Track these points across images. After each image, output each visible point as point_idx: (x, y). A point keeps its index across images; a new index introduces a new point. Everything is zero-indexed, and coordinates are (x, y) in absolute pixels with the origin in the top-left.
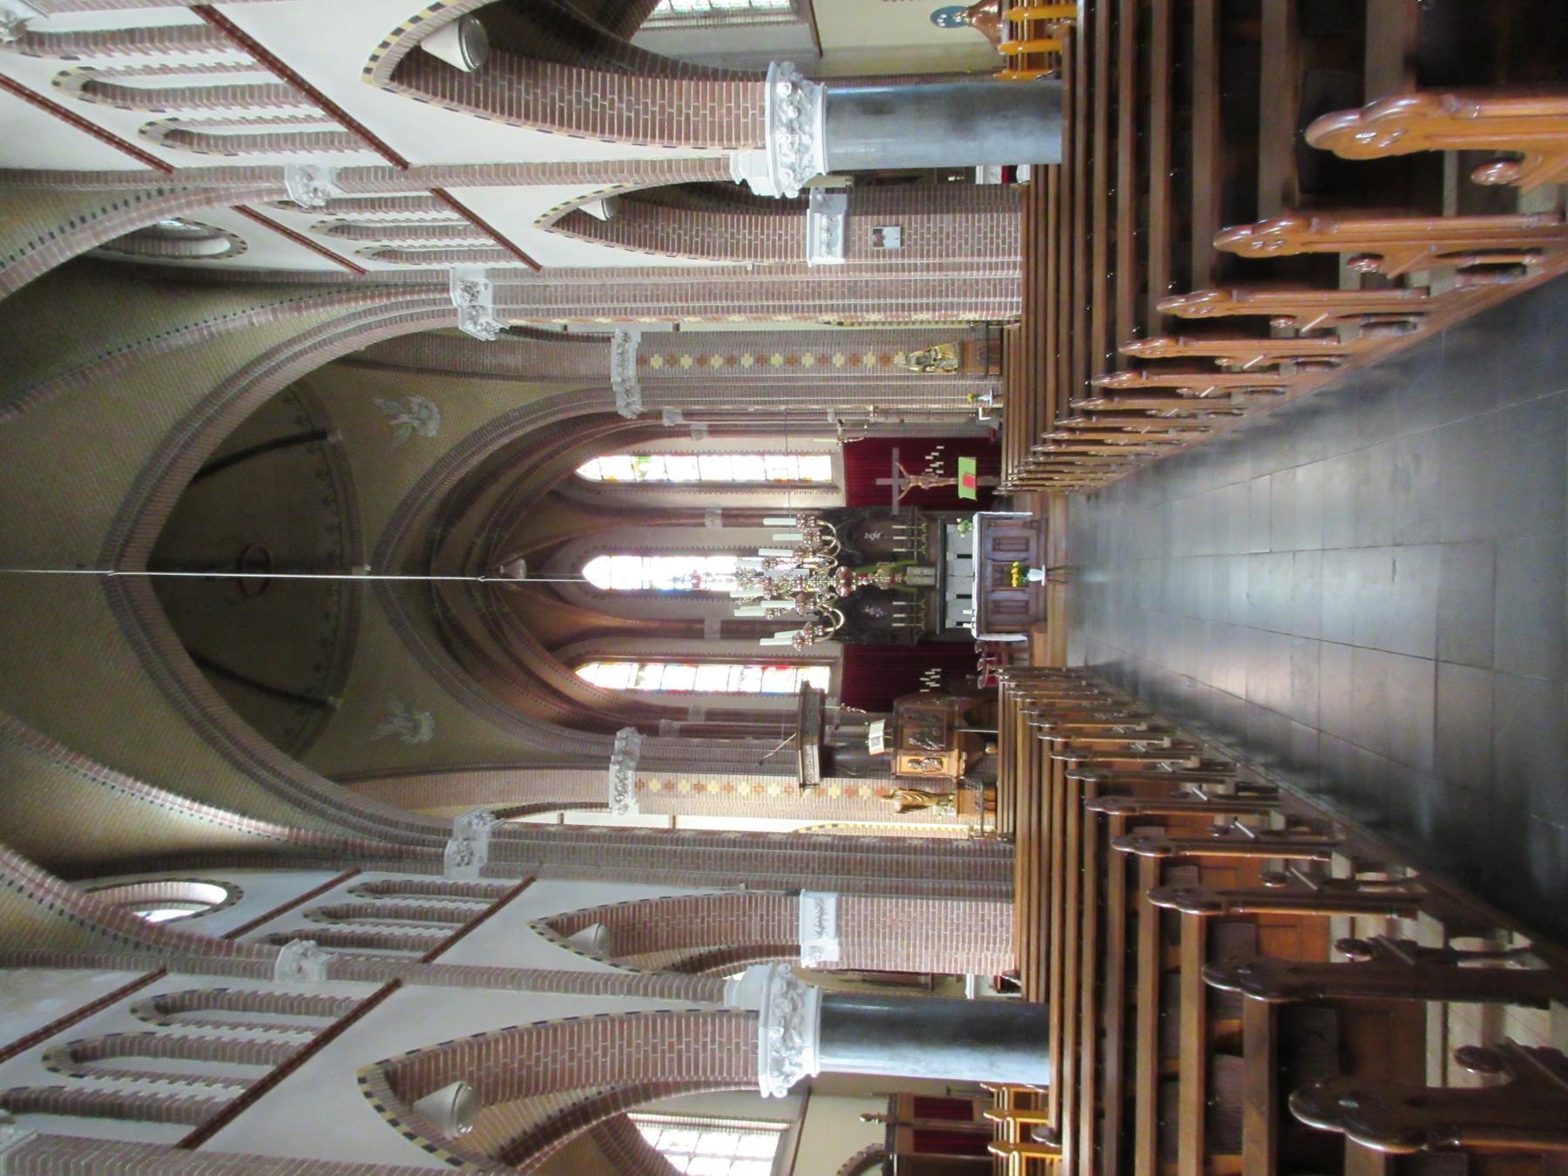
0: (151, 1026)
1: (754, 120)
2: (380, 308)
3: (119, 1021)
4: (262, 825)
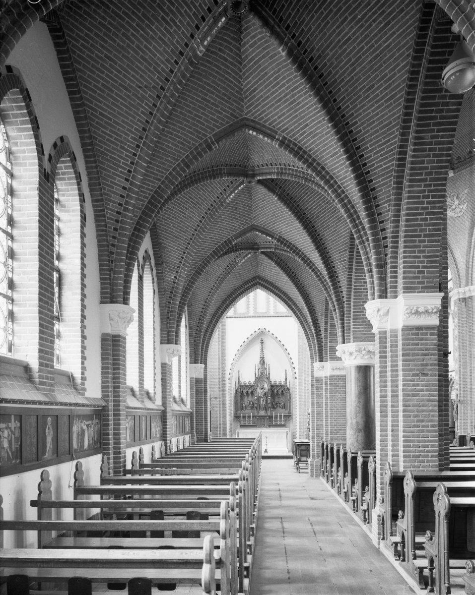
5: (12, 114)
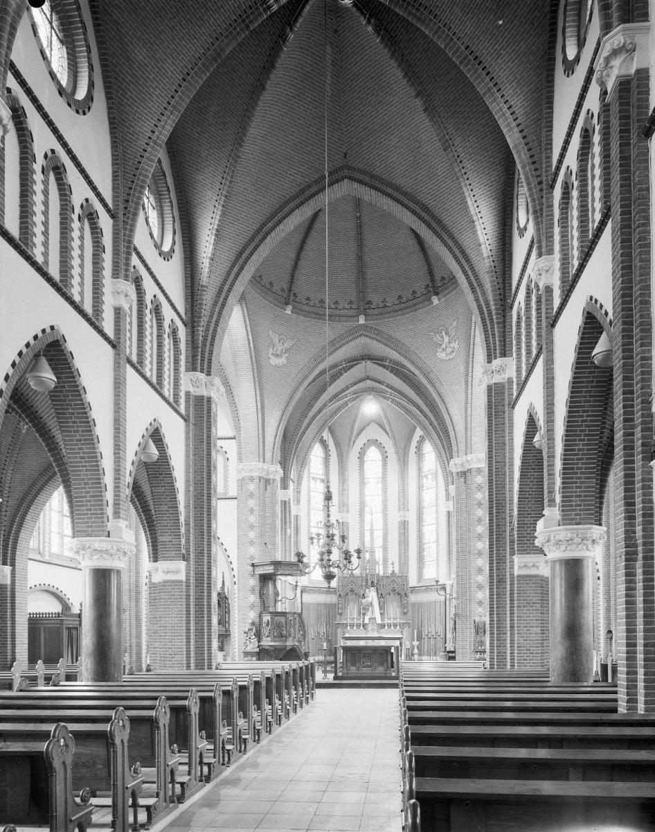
0: (78, 210)
1: (573, 519)
2: (492, 319)
3: (80, 192)
4: (207, 270)
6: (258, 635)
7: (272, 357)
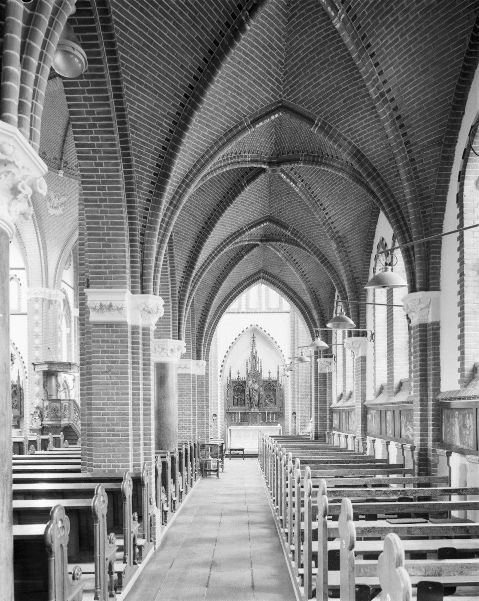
5: (76, 24)
6: (41, 416)
7: (50, 209)
